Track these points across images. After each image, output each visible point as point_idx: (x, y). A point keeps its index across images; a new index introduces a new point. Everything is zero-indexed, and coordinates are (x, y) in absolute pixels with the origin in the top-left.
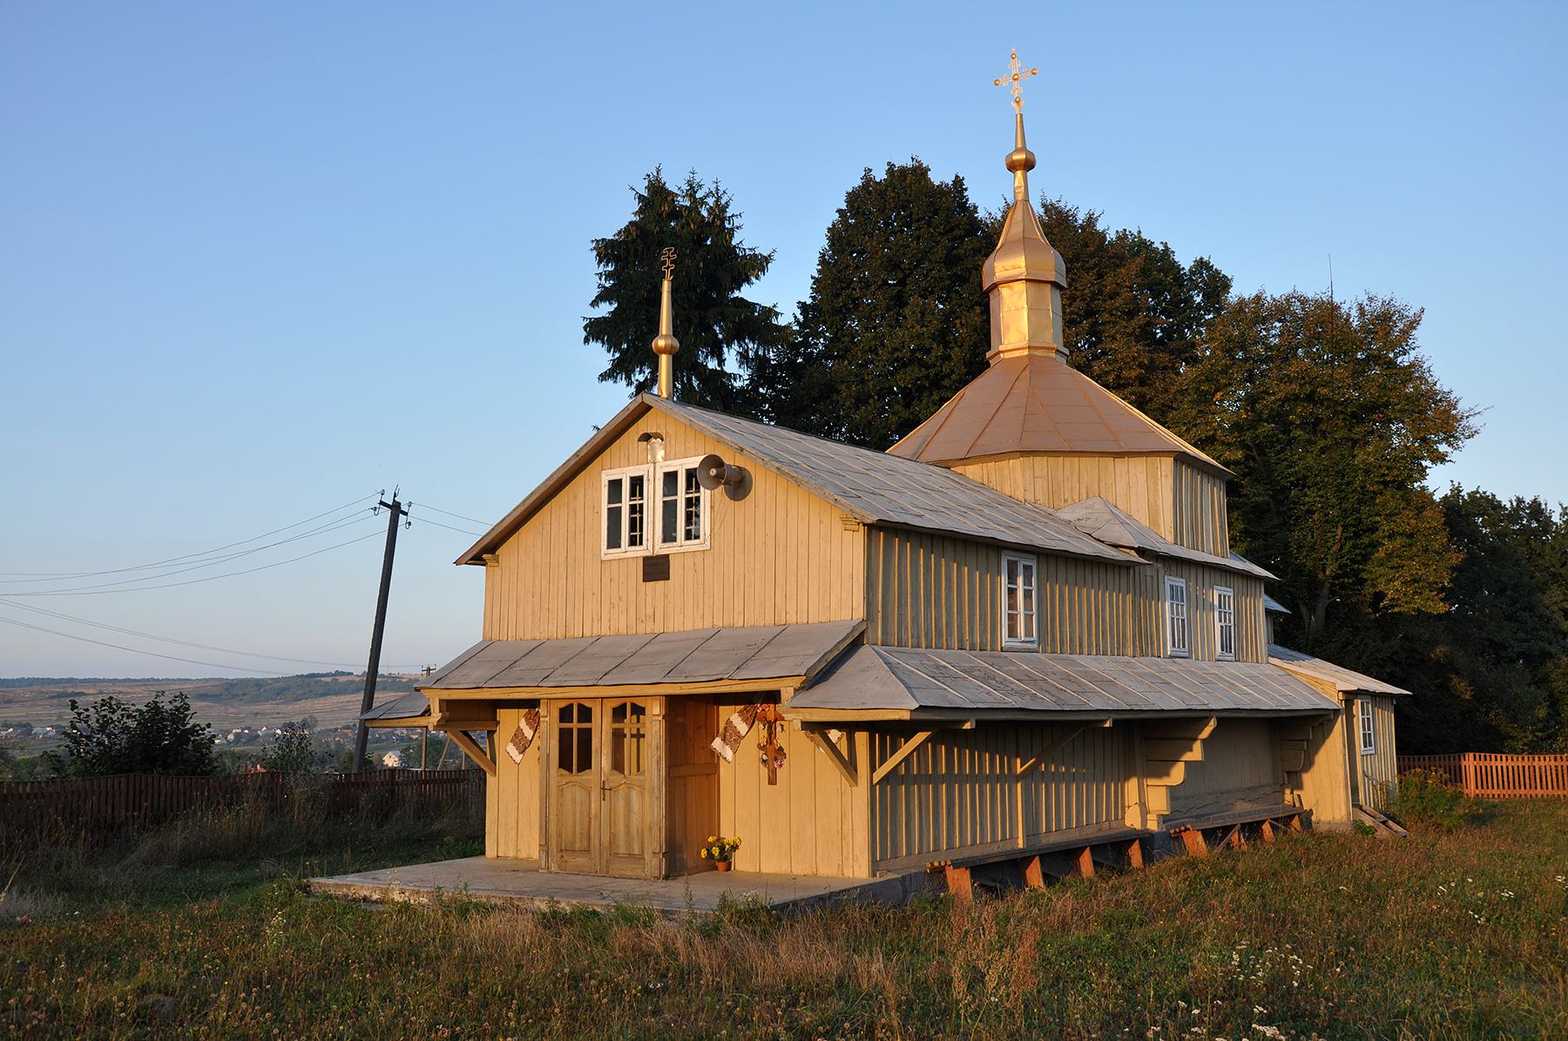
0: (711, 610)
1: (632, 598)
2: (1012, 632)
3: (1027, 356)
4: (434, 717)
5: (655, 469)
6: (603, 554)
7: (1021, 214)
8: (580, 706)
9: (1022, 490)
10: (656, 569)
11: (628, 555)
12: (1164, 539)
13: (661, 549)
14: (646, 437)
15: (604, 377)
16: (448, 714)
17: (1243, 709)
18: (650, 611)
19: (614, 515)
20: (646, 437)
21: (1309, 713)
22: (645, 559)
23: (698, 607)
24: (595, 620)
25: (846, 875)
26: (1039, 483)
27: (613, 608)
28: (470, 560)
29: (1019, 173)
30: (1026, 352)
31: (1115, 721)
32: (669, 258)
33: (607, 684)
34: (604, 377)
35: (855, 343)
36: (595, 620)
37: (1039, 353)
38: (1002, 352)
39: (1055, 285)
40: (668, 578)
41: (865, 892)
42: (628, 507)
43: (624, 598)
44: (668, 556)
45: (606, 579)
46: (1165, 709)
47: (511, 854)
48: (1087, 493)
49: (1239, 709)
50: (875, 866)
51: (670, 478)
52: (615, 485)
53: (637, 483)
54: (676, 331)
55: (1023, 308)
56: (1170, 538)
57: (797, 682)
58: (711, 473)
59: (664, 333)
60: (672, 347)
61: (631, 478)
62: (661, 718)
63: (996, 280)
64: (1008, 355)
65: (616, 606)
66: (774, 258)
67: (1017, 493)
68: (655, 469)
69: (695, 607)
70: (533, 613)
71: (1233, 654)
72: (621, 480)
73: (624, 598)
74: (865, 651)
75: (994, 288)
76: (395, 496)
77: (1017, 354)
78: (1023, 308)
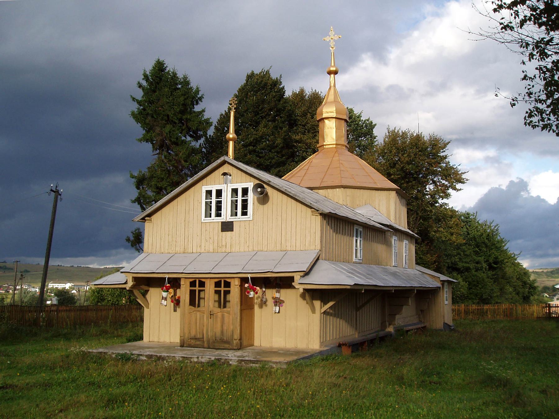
0: (252, 244)
1: (216, 238)
2: (356, 257)
3: (335, 147)
4: (129, 284)
5: (227, 186)
6: (202, 220)
7: (333, 92)
8: (225, 281)
9: (342, 200)
10: (227, 227)
11: (214, 221)
12: (392, 222)
13: (229, 219)
14: (225, 174)
15: (140, 140)
16: (135, 283)
17: (386, 286)
18: (224, 244)
19: (208, 206)
20: (225, 174)
21: (409, 288)
22: (222, 223)
23: (246, 243)
24: (198, 246)
25: (309, 347)
26: (348, 198)
27: (207, 241)
28: (140, 219)
29: (332, 75)
30: (335, 146)
31: (365, 290)
32: (233, 102)
33: (421, 271)
34: (140, 140)
35: (225, 132)
36: (198, 246)
37: (339, 146)
38: (325, 145)
39: (346, 120)
40: (233, 231)
41: (321, 353)
42: (215, 201)
43: (212, 238)
44: (233, 222)
45: (204, 230)
46: (378, 285)
47: (156, 340)
48: (365, 203)
49: (399, 286)
50: (322, 344)
51: (235, 191)
52: (209, 193)
53: (219, 193)
54: (237, 132)
55: (333, 128)
56: (393, 221)
57: (302, 274)
58: (258, 190)
59: (231, 132)
60: (235, 139)
61: (216, 190)
62: (238, 286)
63: (323, 117)
64: (327, 147)
65: (208, 241)
66: (204, 96)
67: (340, 201)
68: (227, 186)
69: (245, 243)
70: (169, 242)
71: (397, 264)
72: (212, 190)
73: (212, 238)
74: (320, 261)
75: (322, 120)
76: (56, 187)
77: (331, 146)
78: (333, 128)
